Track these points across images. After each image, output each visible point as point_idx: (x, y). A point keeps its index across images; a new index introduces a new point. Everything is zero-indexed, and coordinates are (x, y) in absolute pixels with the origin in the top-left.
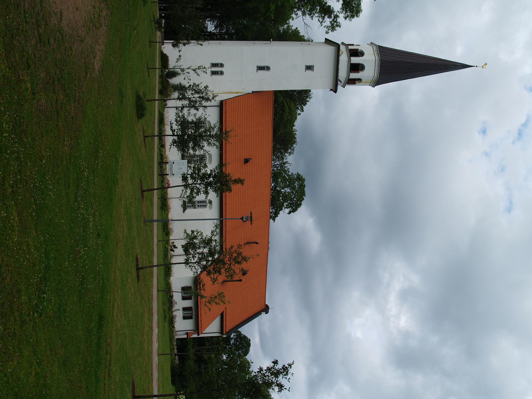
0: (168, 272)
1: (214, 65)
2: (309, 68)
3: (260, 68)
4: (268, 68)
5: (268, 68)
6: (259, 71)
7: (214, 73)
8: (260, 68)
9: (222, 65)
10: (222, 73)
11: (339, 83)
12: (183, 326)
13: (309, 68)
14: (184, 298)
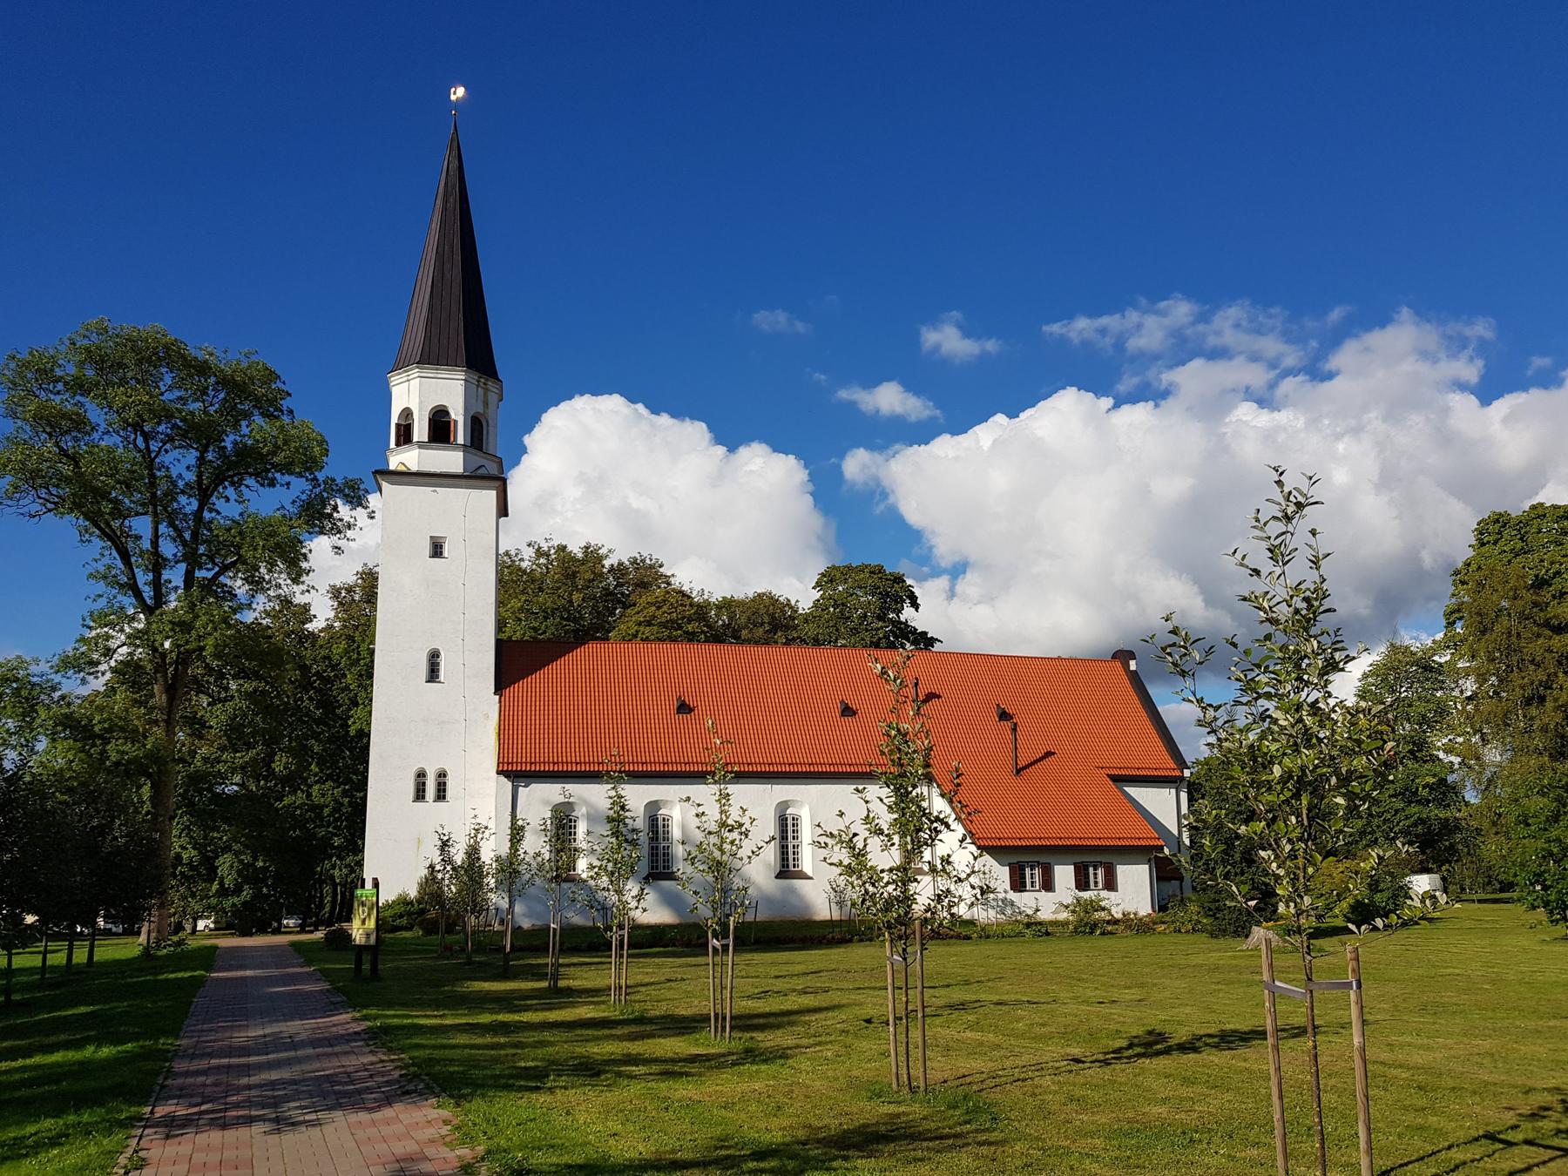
0: (962, 931)
1: (420, 795)
2: (437, 550)
3: (433, 674)
4: (434, 657)
5: (434, 657)
6: (446, 554)
7: (441, 795)
8: (433, 674)
9: (421, 775)
10: (442, 775)
11: (482, 471)
12: (1133, 889)
13: (437, 550)
14: (1048, 885)
